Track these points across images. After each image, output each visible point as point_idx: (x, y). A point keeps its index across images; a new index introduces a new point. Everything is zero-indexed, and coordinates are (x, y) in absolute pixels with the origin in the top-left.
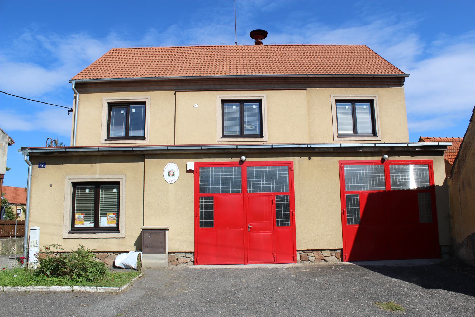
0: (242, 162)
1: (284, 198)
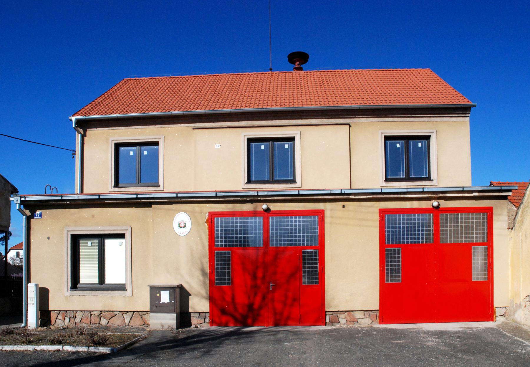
0: (268, 210)
1: (312, 252)
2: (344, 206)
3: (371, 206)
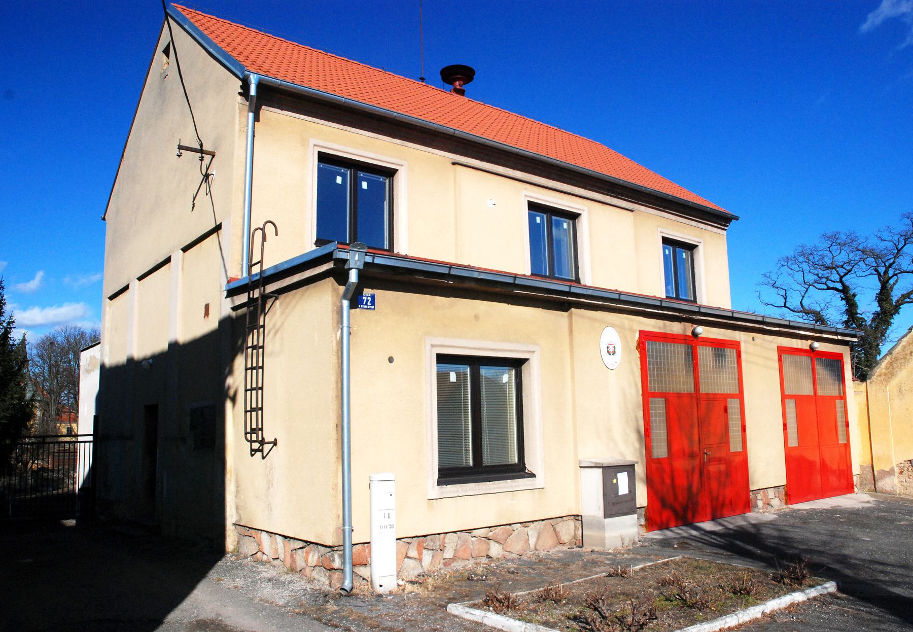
2: (753, 339)
3: (772, 342)
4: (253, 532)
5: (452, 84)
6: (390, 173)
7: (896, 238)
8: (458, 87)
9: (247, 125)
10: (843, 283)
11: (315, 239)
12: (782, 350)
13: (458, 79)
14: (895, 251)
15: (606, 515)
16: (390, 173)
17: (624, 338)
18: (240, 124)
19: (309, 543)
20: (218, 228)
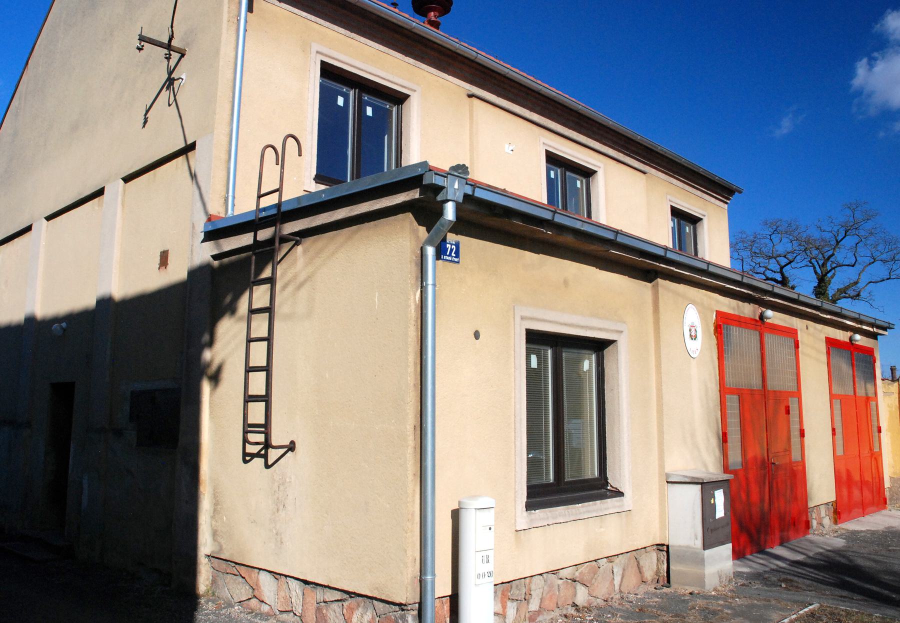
3: (821, 331)
4: (243, 570)
5: (426, 16)
6: (399, 99)
7: (836, 229)
8: (433, 19)
9: (239, 15)
10: (781, 272)
11: (314, 173)
12: (831, 343)
13: (433, 10)
14: (834, 243)
15: (706, 546)
16: (399, 99)
17: (704, 318)
18: (229, 12)
19: (351, 594)
20: (191, 147)
